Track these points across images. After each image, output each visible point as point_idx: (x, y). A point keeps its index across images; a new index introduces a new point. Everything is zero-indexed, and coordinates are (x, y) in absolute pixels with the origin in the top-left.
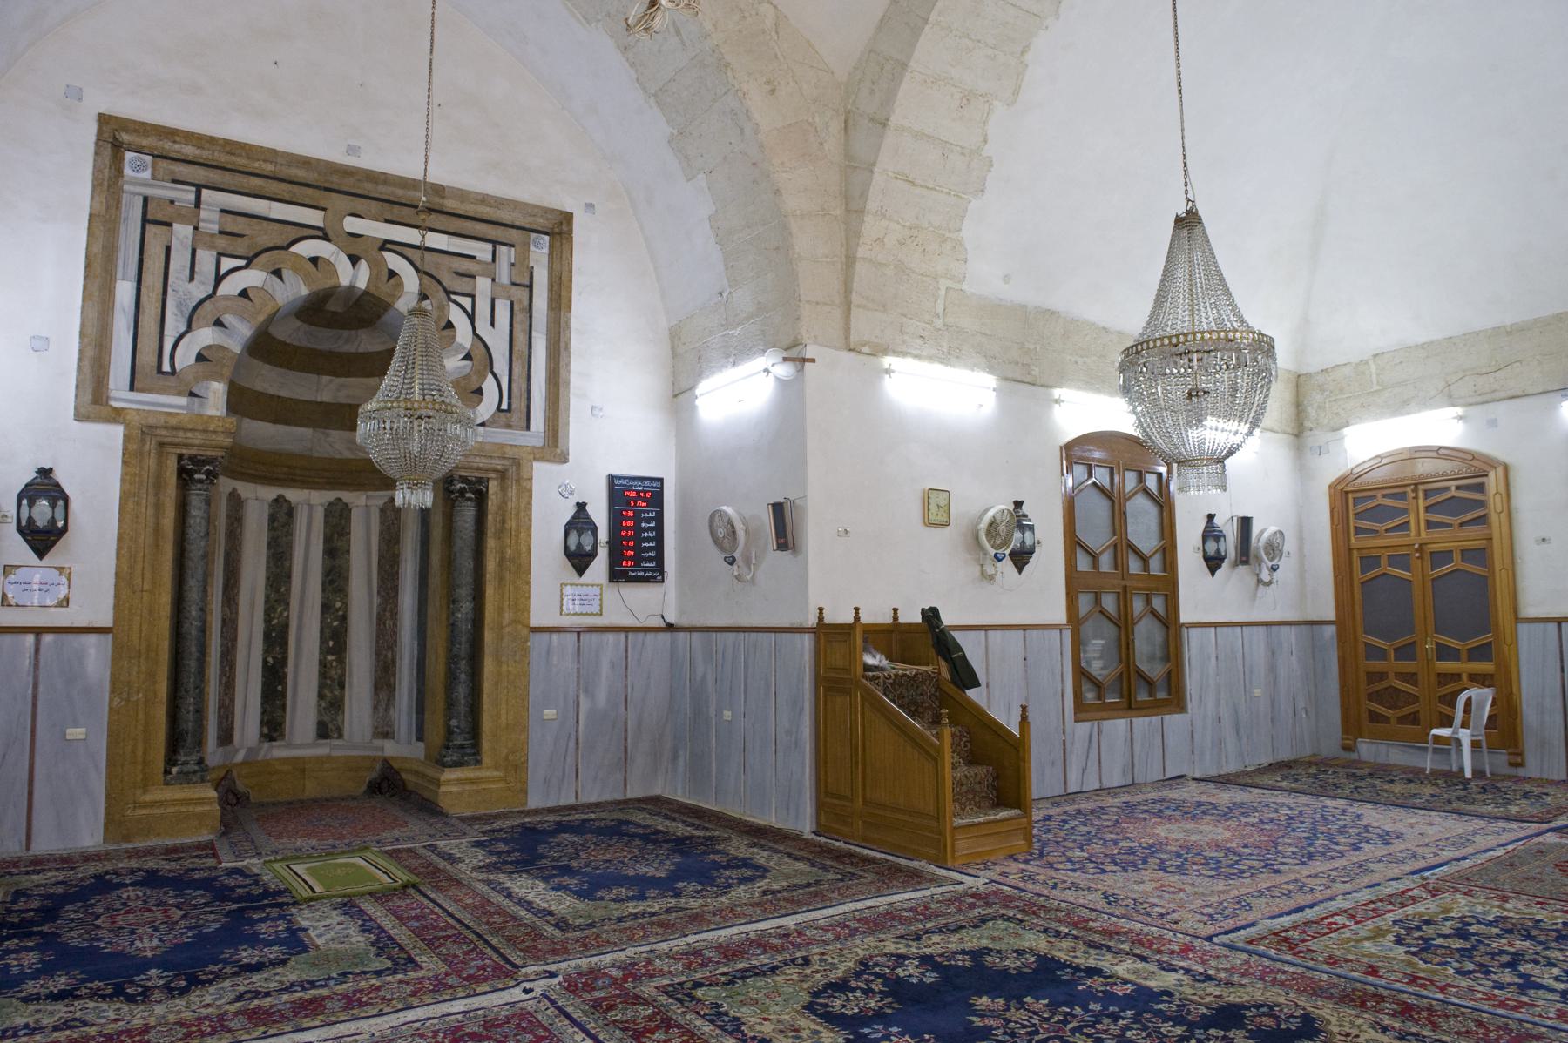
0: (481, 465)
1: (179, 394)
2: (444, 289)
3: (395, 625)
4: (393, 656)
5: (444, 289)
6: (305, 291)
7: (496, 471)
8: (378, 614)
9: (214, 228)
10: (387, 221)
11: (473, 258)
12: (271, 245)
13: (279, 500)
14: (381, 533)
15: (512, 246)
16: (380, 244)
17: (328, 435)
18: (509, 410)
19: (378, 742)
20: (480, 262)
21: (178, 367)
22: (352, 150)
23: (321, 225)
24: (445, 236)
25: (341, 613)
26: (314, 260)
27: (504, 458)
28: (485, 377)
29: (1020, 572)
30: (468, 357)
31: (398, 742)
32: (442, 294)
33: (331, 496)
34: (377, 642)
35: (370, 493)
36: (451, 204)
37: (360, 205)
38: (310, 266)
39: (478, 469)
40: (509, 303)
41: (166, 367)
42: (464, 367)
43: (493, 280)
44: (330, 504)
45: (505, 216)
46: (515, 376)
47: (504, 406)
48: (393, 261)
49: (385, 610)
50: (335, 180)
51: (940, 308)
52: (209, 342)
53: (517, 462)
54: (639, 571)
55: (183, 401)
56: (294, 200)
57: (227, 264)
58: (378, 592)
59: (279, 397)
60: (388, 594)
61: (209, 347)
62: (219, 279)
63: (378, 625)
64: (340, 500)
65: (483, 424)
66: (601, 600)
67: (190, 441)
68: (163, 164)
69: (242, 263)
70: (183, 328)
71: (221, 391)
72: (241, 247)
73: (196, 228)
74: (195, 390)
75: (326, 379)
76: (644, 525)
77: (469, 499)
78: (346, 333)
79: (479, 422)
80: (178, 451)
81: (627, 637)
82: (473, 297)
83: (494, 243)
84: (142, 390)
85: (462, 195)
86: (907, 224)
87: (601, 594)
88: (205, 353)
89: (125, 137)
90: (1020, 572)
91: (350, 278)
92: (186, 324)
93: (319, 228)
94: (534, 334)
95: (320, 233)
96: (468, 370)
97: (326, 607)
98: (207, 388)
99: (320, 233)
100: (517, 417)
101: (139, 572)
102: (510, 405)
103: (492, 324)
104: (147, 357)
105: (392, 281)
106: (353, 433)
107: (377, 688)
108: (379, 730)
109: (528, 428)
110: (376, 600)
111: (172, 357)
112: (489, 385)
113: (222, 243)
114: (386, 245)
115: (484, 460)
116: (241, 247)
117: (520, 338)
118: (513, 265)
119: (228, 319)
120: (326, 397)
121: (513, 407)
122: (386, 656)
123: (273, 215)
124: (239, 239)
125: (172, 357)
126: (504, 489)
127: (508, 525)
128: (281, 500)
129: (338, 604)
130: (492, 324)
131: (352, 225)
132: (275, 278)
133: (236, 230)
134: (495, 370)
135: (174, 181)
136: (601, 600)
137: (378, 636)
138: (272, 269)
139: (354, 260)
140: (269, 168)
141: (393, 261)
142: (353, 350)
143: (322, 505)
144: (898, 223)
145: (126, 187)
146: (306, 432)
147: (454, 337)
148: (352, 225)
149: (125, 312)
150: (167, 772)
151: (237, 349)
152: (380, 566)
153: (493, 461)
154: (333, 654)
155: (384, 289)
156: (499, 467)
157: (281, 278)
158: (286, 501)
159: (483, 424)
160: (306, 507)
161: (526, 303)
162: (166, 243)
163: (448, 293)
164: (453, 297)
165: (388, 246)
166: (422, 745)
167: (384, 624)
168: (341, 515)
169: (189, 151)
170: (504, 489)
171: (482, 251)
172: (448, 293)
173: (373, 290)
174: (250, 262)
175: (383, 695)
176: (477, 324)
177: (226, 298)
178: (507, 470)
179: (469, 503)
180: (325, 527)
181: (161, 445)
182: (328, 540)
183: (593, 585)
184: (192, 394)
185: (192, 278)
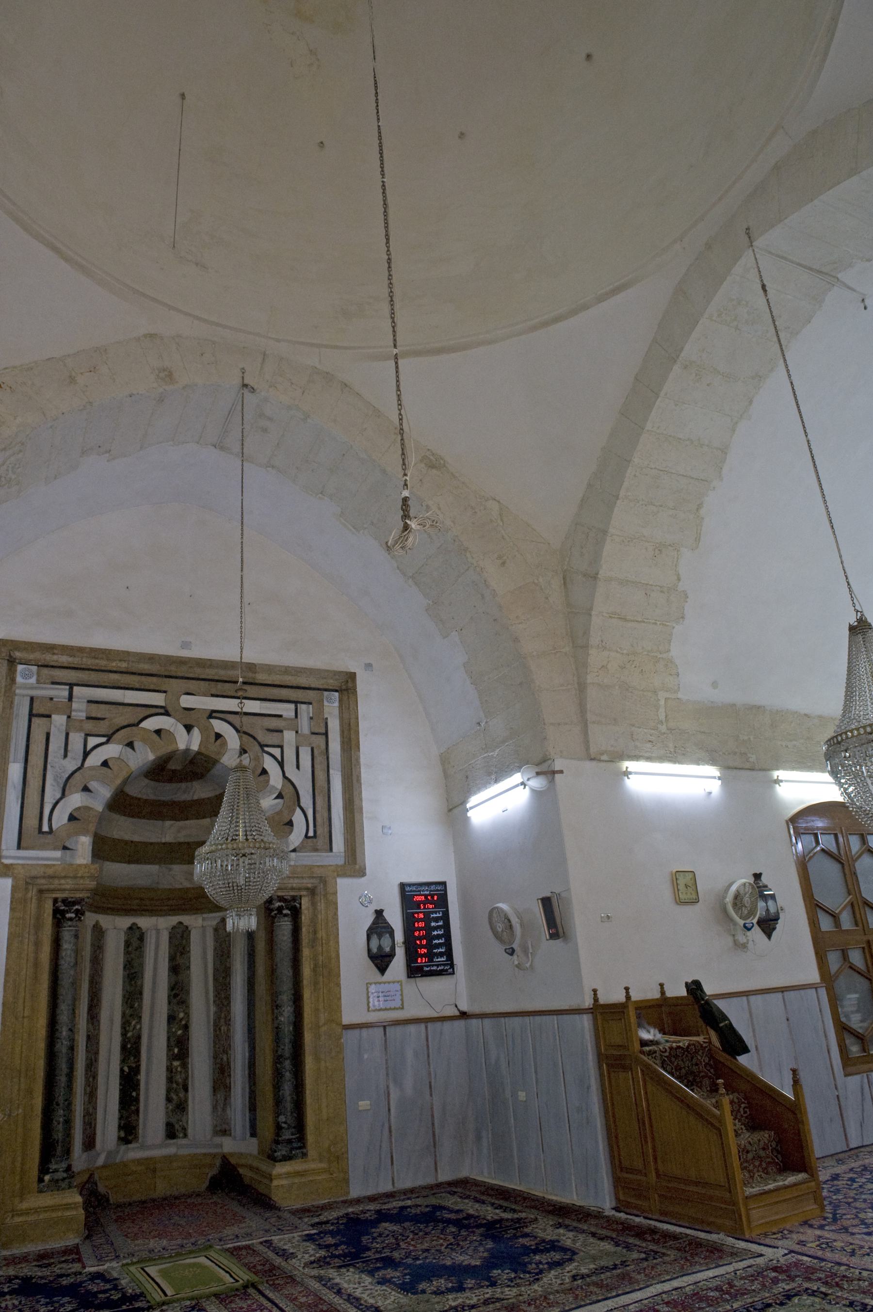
0: (295, 885)
1: (55, 849)
2: (259, 743)
3: (229, 1030)
4: (228, 1059)
5: (259, 743)
6: (151, 757)
7: (307, 889)
8: (215, 1021)
9: (83, 715)
10: (213, 696)
11: (281, 716)
12: (125, 724)
13: (133, 928)
14: (215, 949)
15: (310, 703)
16: (208, 714)
17: (170, 870)
18: (315, 836)
19: (218, 1140)
20: (286, 719)
21: (54, 827)
22: (186, 645)
23: (163, 704)
24: (258, 702)
25: (183, 1022)
26: (158, 732)
27: (313, 877)
28: (294, 811)
29: (769, 936)
30: (280, 796)
31: (235, 1138)
32: (258, 748)
33: (174, 920)
34: (214, 1047)
35: (205, 916)
36: (261, 677)
37: (192, 685)
38: (155, 736)
39: (293, 889)
40: (310, 749)
41: (45, 828)
42: (277, 804)
43: (297, 732)
44: (174, 928)
45: (303, 681)
46: (318, 808)
47: (311, 834)
48: (219, 726)
49: (219, 1018)
50: (173, 670)
51: (662, 717)
52: (79, 805)
53: (323, 880)
54: (433, 966)
55: (58, 854)
56: (142, 687)
57: (92, 741)
58: (214, 1002)
59: (132, 842)
60: (222, 1002)
61: (78, 809)
62: (86, 754)
63: (215, 1030)
64: (181, 923)
65: (294, 851)
66: (402, 995)
67: (63, 887)
68: (45, 671)
69: (104, 739)
70: (58, 796)
71: (87, 843)
72: (103, 727)
73: (69, 717)
74: (67, 845)
75: (168, 823)
76: (433, 924)
77: (286, 915)
78: (183, 785)
79: (292, 847)
80: (54, 896)
81: (426, 1027)
82: (281, 747)
83: (296, 703)
84: (27, 848)
85: (270, 669)
86: (625, 652)
87: (401, 990)
88: (75, 814)
89: (18, 654)
90: (769, 936)
91: (186, 743)
92: (61, 792)
93: (161, 707)
94: (331, 771)
95: (162, 711)
96: (280, 807)
97: (171, 1019)
98: (77, 842)
99: (162, 711)
100: (321, 842)
101: (21, 1001)
102: (315, 832)
103: (298, 767)
104: (31, 822)
105: (219, 741)
106: (191, 866)
107: (215, 1090)
108: (218, 1129)
109: (331, 850)
110: (213, 1009)
111: (50, 819)
112: (298, 818)
113: (90, 726)
114: (213, 714)
115: (296, 881)
116: (103, 727)
117: (321, 776)
118: (311, 718)
119: (93, 785)
120: (168, 838)
121: (318, 833)
122: (222, 1059)
123: (127, 701)
124: (102, 722)
125: (50, 819)
126: (314, 904)
127: (319, 935)
128: (134, 927)
129: (181, 1015)
130: (298, 767)
131: (187, 701)
132: (129, 749)
133: (99, 716)
134: (302, 804)
135: (53, 683)
136: (402, 995)
137: (214, 1042)
138: (126, 742)
139: (189, 728)
140: (123, 665)
141: (219, 726)
142: (189, 798)
143: (167, 929)
144: (617, 652)
145: (17, 691)
146: (154, 868)
147: (268, 781)
148: (187, 701)
149: (15, 787)
150: (41, 1180)
151: (100, 808)
152: (215, 979)
153: (305, 881)
154: (177, 1060)
155: (212, 749)
156: (309, 886)
157: (133, 748)
158: (139, 928)
159: (294, 851)
160: (154, 932)
161: (323, 747)
162: (46, 730)
163: (262, 746)
164: (266, 749)
165: (214, 715)
166: (254, 1140)
167: (220, 1029)
168: (182, 937)
169: (64, 659)
170: (314, 904)
171: (287, 710)
172: (262, 746)
173: (203, 751)
174: (109, 738)
175: (220, 1096)
176: (286, 769)
177: (92, 768)
178: (316, 887)
179: (286, 919)
180: (170, 947)
181: (41, 891)
182: (172, 959)
183: (394, 982)
184: (65, 848)
185: (65, 756)
